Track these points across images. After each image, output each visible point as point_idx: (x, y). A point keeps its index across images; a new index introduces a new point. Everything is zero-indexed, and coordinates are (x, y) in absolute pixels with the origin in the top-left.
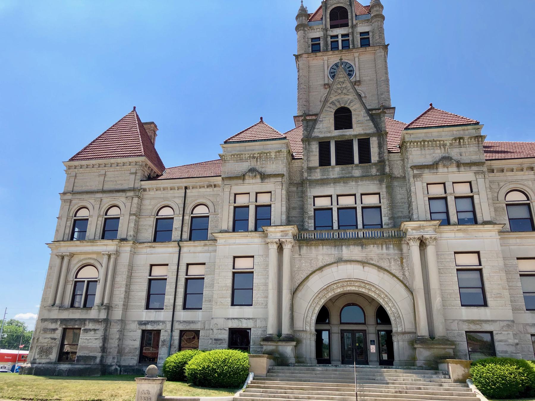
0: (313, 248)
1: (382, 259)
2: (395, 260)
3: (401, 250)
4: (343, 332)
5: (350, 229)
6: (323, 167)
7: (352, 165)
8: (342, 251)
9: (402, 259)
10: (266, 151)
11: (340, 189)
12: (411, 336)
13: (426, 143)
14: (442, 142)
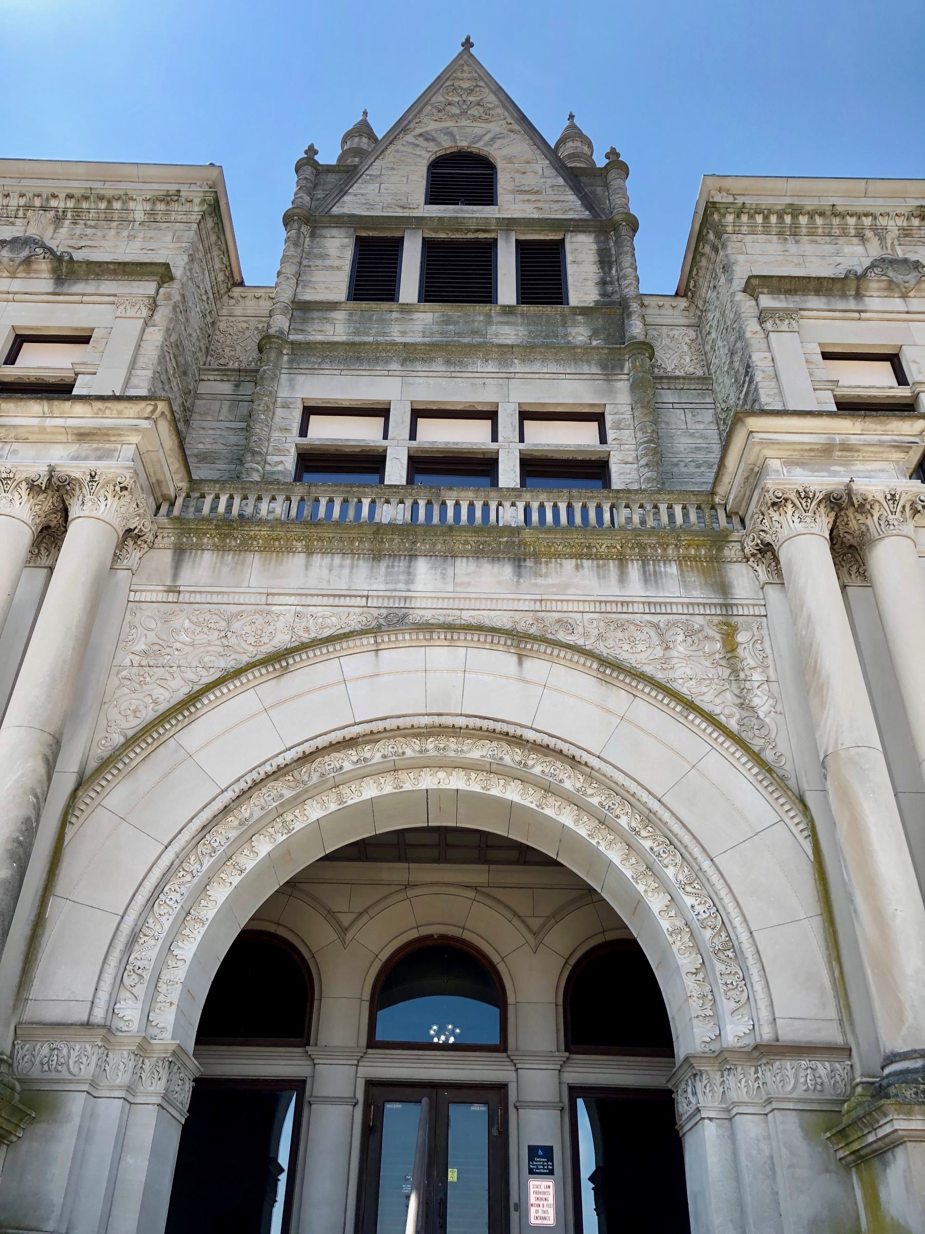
0: (254, 561)
1: (622, 627)
2: (690, 633)
3: (724, 588)
4: (379, 1092)
5: (464, 487)
6: (364, 305)
7: (486, 308)
8: (410, 581)
9: (729, 634)
10: (109, 190)
11: (432, 386)
12: (823, 1068)
13: (803, 220)
14: (867, 221)
